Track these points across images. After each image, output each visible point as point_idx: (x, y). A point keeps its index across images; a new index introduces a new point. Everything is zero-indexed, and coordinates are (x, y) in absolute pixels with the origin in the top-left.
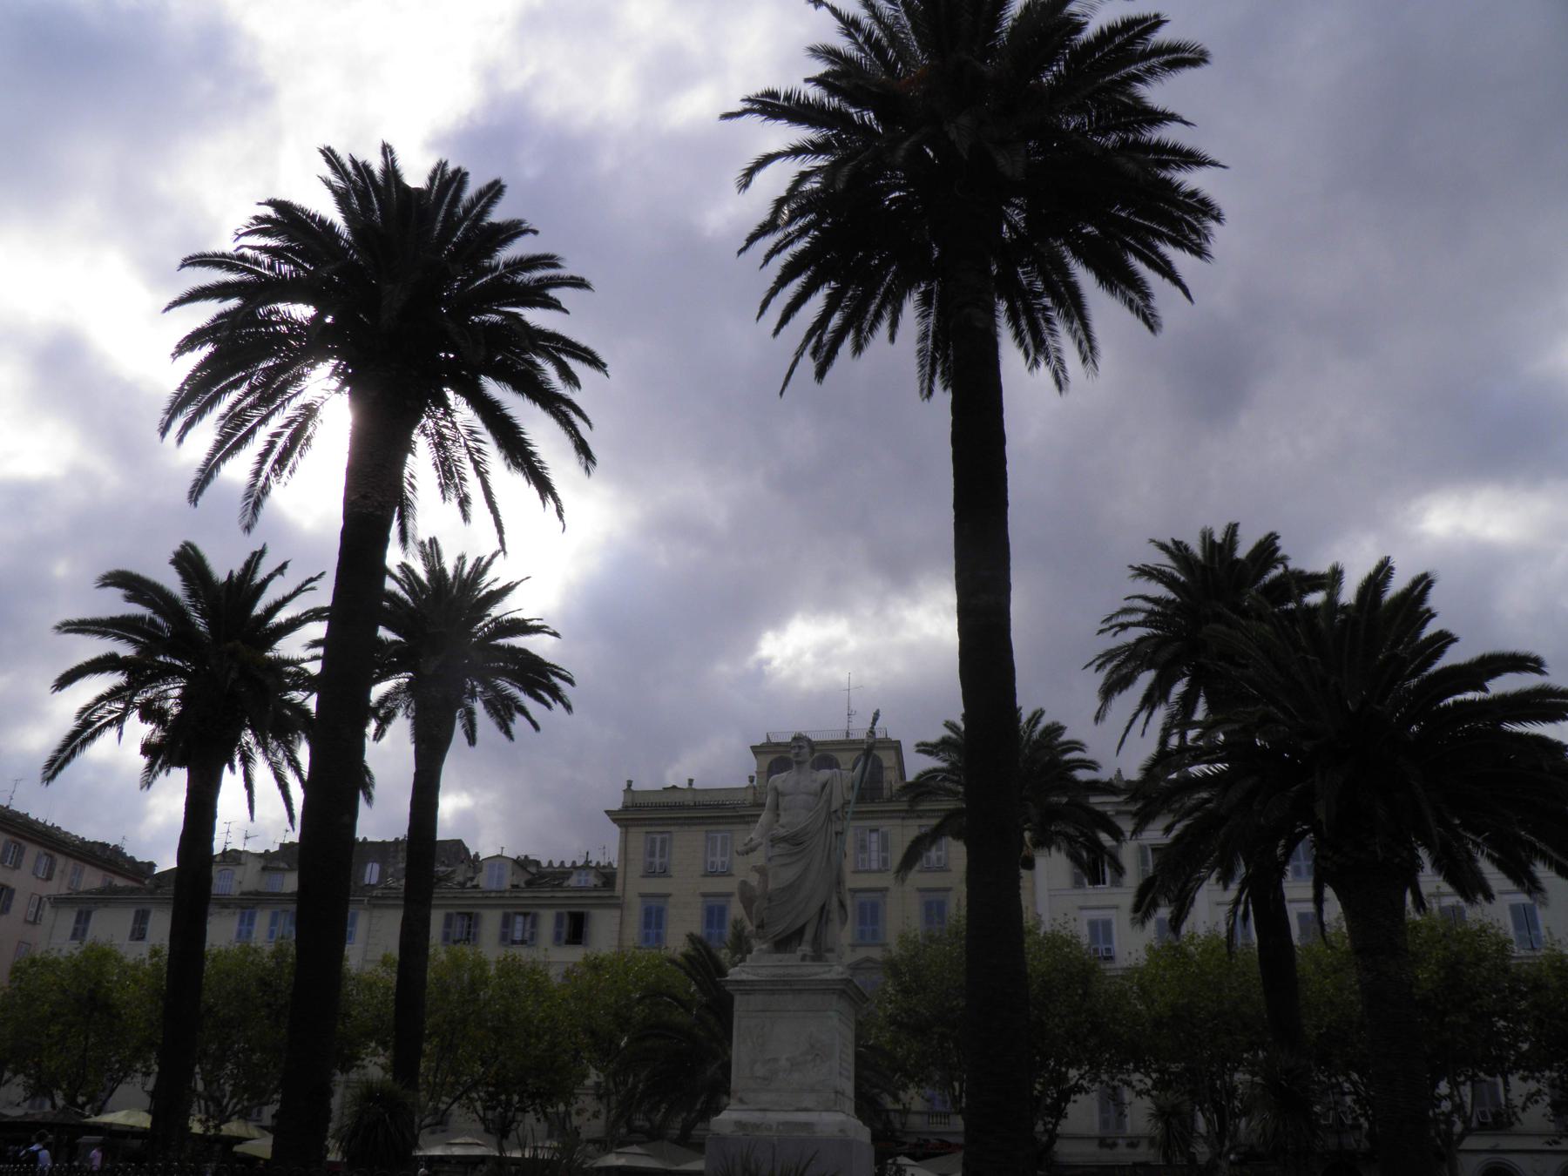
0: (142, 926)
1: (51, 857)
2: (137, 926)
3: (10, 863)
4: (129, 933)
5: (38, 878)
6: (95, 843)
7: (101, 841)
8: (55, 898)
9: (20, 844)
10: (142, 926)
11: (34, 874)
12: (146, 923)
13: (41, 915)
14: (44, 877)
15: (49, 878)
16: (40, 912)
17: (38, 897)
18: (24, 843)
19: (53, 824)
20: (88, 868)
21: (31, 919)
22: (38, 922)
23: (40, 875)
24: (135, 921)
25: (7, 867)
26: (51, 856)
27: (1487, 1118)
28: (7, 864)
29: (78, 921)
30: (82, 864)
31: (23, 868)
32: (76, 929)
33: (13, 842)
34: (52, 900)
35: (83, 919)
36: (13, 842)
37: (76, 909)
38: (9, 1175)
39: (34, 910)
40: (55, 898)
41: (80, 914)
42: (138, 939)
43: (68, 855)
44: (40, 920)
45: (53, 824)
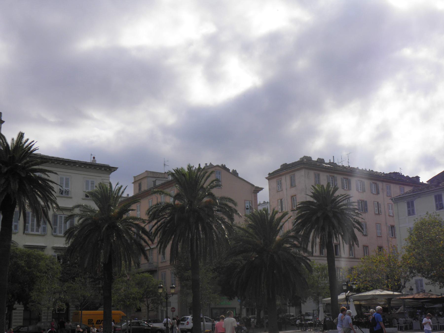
0: (440, 202)
1: (376, 184)
2: (438, 203)
3: (347, 188)
4: (435, 208)
5: (373, 194)
6: (390, 173)
7: (393, 172)
8: (395, 199)
9: (347, 179)
10: (440, 202)
11: (372, 193)
12: (442, 201)
13: (381, 210)
14: (376, 193)
15: (378, 193)
16: (380, 209)
17: (377, 203)
18: (335, 175)
19: (369, 170)
20: (392, 186)
21: (377, 213)
22: (380, 213)
23: (360, 191)
24: (436, 201)
25: (345, 190)
26: (376, 184)
27: (248, 207)
28: (345, 189)
29: (408, 207)
30: (389, 184)
31: (380, 193)
32: (409, 211)
33: (330, 176)
34: (393, 200)
35: (411, 205)
36: (330, 176)
37: (406, 201)
38: (443, 276)
39: (377, 208)
40: (395, 199)
41: (408, 204)
42: (441, 209)
43: (383, 181)
44: (381, 213)
45: (369, 170)
